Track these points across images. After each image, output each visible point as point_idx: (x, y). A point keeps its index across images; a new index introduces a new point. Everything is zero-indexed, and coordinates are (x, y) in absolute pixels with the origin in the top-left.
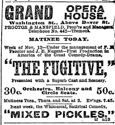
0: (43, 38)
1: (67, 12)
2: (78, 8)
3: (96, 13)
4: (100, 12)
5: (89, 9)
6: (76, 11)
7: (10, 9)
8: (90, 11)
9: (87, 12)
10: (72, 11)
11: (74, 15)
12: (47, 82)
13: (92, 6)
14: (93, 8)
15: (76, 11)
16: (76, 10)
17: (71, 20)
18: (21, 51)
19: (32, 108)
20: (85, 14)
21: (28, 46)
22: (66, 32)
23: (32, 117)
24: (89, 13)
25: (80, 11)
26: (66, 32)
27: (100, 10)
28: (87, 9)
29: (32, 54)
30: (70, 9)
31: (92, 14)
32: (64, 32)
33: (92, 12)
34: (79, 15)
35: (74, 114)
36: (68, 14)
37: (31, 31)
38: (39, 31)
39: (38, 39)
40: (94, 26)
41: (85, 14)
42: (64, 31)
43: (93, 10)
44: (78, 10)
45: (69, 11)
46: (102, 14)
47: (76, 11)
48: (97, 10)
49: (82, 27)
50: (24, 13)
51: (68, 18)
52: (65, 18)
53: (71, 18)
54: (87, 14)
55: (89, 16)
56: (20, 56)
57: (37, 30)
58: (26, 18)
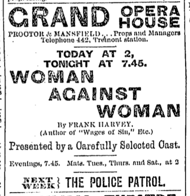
1: (122, 16)
2: (139, 9)
3: (168, 17)
4: (174, 16)
5: (156, 11)
6: (136, 15)
8: (156, 14)
10: (130, 15)
11: (133, 21)
13: (159, 7)
14: (40, 13)
16: (135, 14)
17: (128, 29)
18: (129, 39)
21: (88, 123)
22: (86, 42)
23: (164, 116)
24: (157, 18)
25: (142, 15)
26: (86, 42)
27: (174, 13)
28: (152, 11)
29: (142, 37)
31: (162, 20)
32: (83, 42)
34: (141, 20)
35: (30, 17)
36: (125, 19)
37: (45, 40)
38: (57, 41)
41: (150, 19)
42: (84, 39)
43: (162, 13)
44: (138, 13)
45: (125, 15)
47: (129, 19)
48: (168, 12)
49: (133, 34)
51: (125, 26)
52: (121, 27)
53: (128, 26)
55: (157, 22)
57: (57, 37)
58: (53, 25)
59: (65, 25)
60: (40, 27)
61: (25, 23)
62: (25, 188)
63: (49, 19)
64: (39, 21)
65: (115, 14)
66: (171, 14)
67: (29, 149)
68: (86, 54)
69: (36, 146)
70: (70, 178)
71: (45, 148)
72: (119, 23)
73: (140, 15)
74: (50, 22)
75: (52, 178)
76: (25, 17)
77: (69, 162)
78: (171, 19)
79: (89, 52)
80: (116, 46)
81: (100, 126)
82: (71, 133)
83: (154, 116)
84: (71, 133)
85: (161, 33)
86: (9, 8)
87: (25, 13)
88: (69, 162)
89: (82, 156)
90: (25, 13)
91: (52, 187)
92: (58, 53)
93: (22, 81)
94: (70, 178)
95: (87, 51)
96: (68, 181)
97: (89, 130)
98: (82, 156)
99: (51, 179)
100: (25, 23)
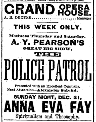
0: (34, 35)
3: (83, 11)
4: (87, 10)
5: (77, 7)
6: (67, 9)
8: (78, 9)
9: (76, 10)
12: (28, 37)
13: (79, 5)
15: (67, 9)
19: (50, 85)
20: (74, 11)
24: (78, 10)
25: (70, 9)
27: (87, 8)
30: (62, 7)
33: (79, 9)
35: (15, 9)
36: (61, 11)
39: (38, 48)
40: (79, 18)
41: (74, 11)
44: (68, 8)
46: (88, 11)
48: (84, 8)
51: (61, 14)
53: (63, 15)
54: (76, 11)
55: (77, 13)
56: (18, 91)
58: (26, 13)
59: (33, 13)
60: (20, 14)
61: (13, 12)
63: (25, 10)
64: (20, 11)
65: (57, 8)
66: (85, 9)
67: (61, 116)
68: (33, 97)
69: (49, 117)
70: (17, 25)
71: (63, 118)
72: (44, 69)
73: (69, 9)
74: (24, 12)
75: (41, 48)
76: (13, 9)
78: (85, 11)
79: (34, 96)
80: (58, 32)
82: (62, 27)
84: (62, 27)
85: (83, 19)
86: (5, 4)
87: (13, 7)
89: (2, 95)
90: (13, 7)
92: (15, 26)
94: (17, 25)
95: (33, 96)
98: (2, 95)
100: (13, 12)
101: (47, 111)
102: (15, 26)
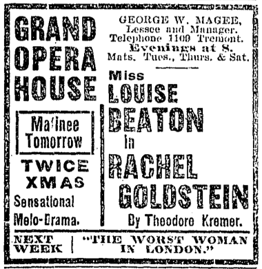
1: (136, 17)
7: (22, 22)
21: (241, 243)
50: (45, 29)
62: (18, 251)
77: (198, 18)
81: (126, 147)
83: (62, 187)
88: (198, 18)
91: (59, 251)
92: (24, 164)
93: (46, 163)
96: (29, 138)
97: (207, 216)
99: (50, 238)
101: (59, 68)
102: (24, 164)
